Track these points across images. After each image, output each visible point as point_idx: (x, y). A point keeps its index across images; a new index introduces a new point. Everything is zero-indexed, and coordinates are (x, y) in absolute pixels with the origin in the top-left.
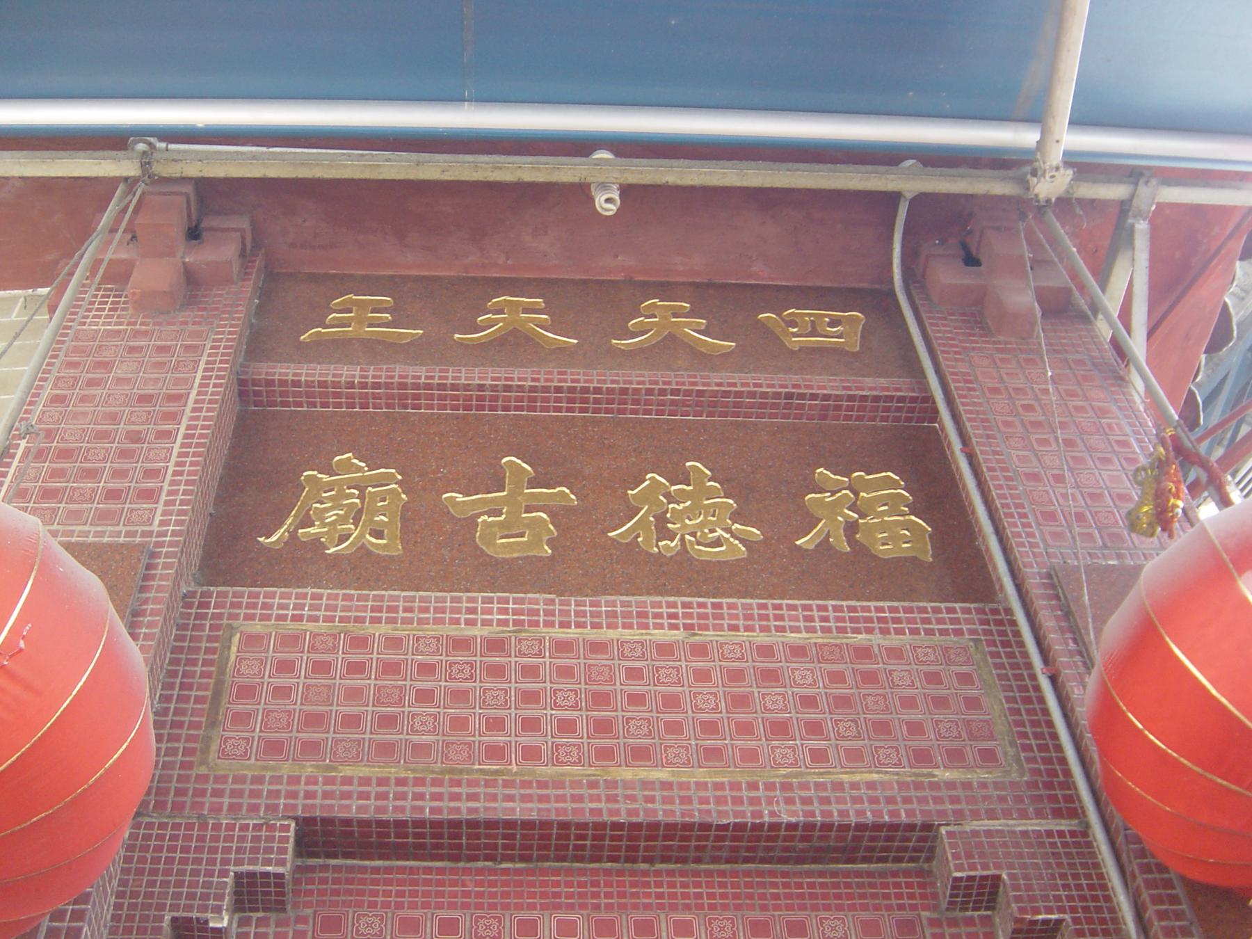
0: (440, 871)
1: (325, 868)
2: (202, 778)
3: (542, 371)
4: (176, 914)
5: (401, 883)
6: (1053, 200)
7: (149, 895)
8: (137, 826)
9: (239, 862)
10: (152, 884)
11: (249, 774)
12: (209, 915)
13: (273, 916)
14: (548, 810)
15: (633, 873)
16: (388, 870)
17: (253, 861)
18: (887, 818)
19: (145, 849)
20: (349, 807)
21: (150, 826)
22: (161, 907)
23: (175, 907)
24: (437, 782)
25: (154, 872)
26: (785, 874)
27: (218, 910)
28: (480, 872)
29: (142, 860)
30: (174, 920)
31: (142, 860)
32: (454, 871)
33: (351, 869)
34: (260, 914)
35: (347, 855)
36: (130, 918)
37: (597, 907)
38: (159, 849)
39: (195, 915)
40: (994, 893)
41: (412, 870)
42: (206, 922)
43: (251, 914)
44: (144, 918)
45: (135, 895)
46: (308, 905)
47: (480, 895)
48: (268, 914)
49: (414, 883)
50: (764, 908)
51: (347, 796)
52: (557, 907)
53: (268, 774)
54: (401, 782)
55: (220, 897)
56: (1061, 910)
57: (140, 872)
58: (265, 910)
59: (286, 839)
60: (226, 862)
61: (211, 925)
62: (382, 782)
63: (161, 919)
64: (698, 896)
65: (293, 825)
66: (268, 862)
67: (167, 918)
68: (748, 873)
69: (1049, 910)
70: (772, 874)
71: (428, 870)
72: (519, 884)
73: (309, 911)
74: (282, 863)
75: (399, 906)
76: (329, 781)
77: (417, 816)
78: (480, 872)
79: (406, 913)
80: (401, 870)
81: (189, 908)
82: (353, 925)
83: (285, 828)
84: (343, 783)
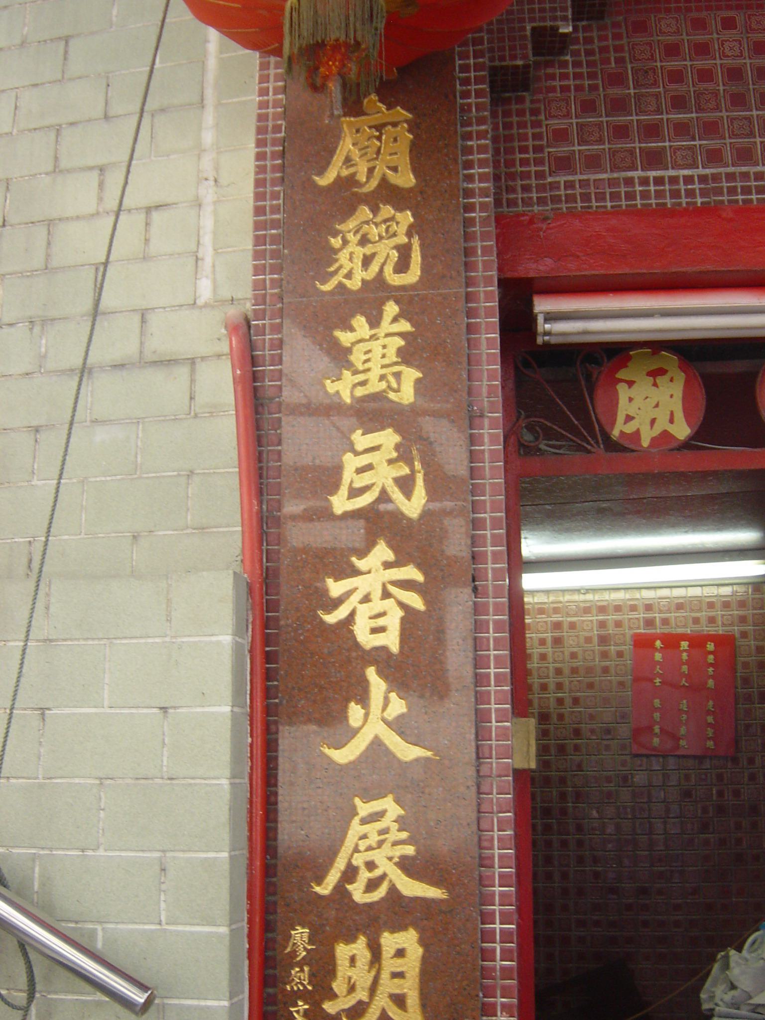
3: (594, 209)
4: (534, 25)
6: (381, 206)
12: (560, 23)
13: (594, 24)
18: (510, 832)
22: (521, 20)
23: (532, 20)
27: (565, 19)
30: (533, 29)
34: (584, 23)
39: (549, 23)
40: (467, 312)
42: (558, 29)
43: (578, 23)
48: (590, 22)
58: (588, 19)
61: (561, 31)
63: (523, 29)
67: (529, 28)
73: (621, 18)
75: (689, 10)
79: (694, 14)
82: (656, 25)
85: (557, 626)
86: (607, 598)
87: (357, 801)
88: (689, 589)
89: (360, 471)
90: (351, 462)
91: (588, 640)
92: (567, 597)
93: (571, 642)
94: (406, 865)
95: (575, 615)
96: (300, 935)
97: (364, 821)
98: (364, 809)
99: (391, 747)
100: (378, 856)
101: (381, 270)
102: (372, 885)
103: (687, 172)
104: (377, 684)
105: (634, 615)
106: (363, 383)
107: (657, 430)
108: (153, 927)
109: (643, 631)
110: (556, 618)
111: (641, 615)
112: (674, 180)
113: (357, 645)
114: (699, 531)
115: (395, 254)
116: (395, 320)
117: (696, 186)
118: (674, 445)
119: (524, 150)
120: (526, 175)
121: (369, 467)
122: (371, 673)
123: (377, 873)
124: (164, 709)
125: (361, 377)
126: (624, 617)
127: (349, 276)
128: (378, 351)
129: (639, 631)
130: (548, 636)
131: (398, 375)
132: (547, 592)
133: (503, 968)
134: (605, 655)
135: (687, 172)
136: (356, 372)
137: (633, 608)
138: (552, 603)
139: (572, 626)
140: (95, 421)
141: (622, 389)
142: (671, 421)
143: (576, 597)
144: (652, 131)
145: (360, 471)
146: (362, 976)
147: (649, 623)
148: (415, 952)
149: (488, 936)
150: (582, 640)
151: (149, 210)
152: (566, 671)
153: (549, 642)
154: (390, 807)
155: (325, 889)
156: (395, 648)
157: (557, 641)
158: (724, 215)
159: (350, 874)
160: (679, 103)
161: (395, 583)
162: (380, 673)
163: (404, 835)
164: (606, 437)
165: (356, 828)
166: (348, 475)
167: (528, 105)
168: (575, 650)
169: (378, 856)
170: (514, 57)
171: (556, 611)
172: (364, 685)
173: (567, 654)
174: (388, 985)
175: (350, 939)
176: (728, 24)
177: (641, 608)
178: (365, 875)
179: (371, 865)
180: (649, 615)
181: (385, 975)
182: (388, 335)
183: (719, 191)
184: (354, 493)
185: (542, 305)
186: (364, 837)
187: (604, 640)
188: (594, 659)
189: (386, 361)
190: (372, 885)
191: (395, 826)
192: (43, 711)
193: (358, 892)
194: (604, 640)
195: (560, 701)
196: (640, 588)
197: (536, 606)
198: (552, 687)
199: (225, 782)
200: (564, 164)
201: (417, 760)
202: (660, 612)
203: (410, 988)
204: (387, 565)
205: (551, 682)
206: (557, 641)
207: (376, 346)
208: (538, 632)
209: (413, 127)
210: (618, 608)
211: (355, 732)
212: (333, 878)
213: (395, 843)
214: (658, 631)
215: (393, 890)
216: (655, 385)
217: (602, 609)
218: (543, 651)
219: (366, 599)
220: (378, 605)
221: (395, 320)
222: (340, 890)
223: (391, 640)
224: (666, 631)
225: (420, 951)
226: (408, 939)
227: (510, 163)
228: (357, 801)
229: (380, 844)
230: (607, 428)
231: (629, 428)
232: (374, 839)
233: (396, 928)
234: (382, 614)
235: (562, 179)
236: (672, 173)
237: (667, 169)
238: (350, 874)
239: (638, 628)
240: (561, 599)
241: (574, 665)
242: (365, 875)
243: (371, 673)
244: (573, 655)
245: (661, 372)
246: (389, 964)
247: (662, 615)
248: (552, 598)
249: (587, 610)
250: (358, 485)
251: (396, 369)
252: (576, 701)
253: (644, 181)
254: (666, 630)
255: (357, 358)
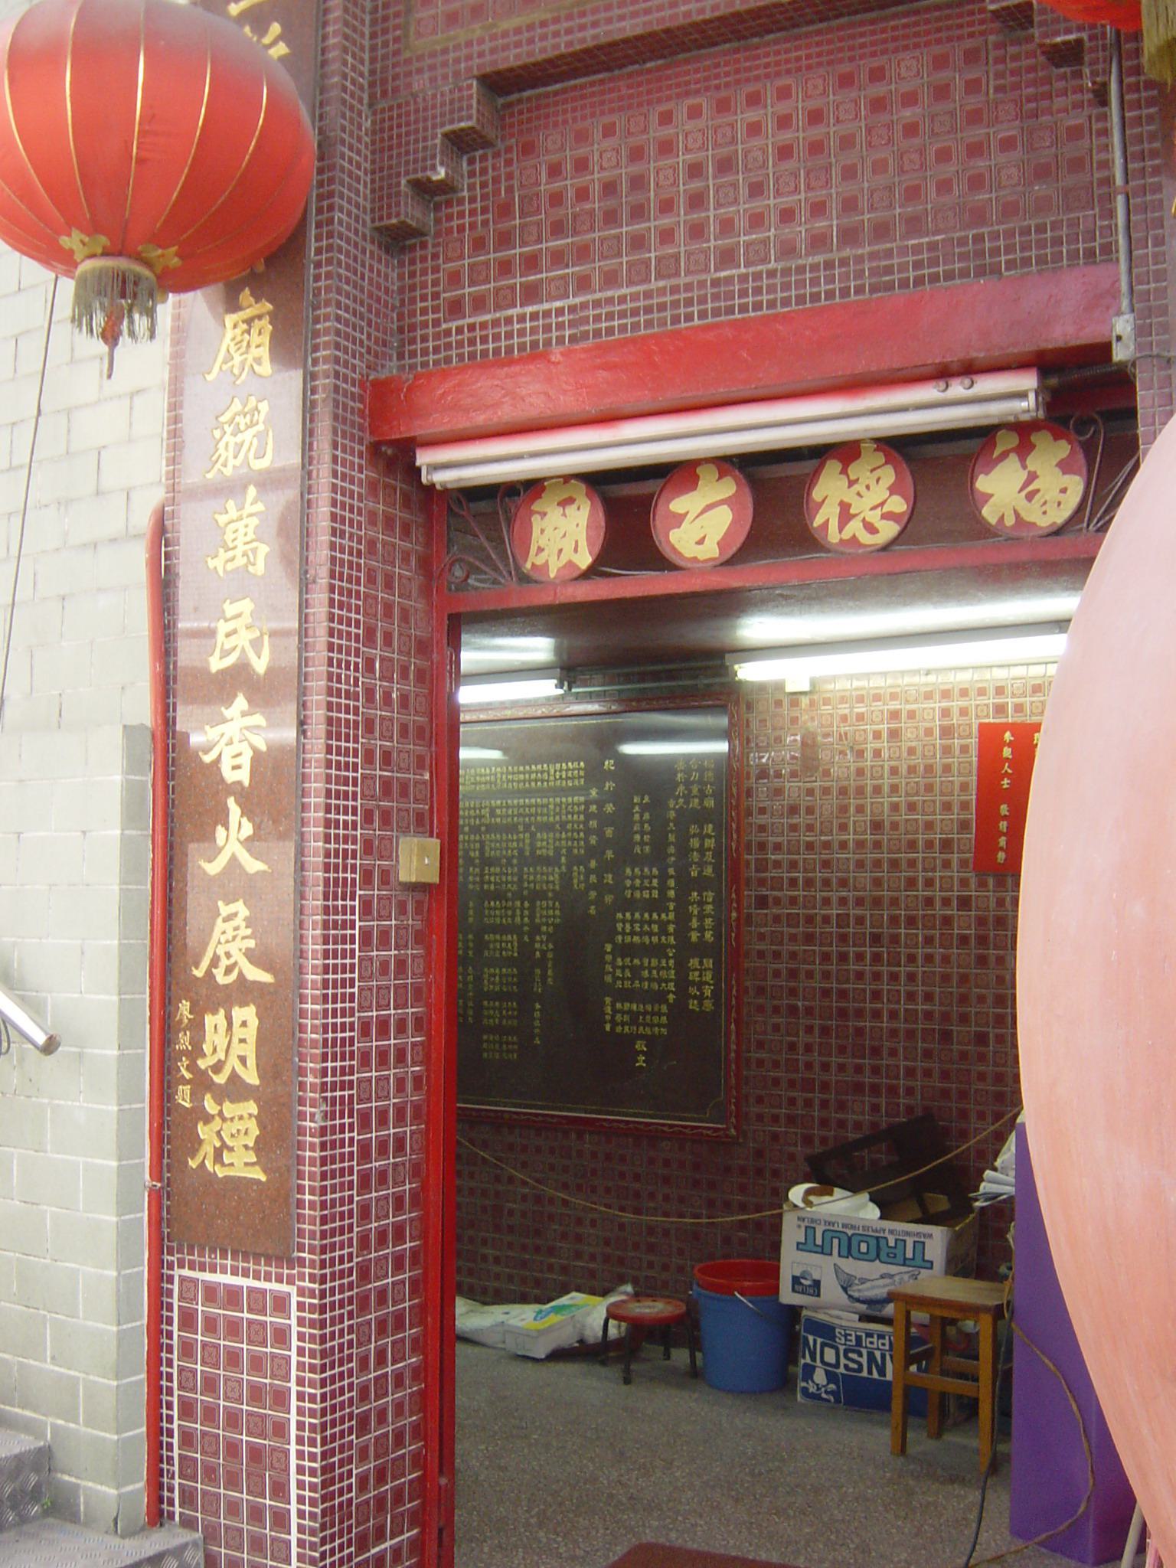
0: (602, 82)
1: (520, 101)
2: (408, 61)
5: (574, 100)
7: (390, 167)
8: (375, 113)
9: (443, 125)
10: (390, 157)
11: (438, 48)
12: (429, 173)
14: (651, 23)
15: (746, 49)
16: (564, 91)
17: (452, 122)
19: (382, 130)
20: (507, 59)
21: (383, 111)
22: (398, 175)
24: (570, 17)
25: (390, 148)
26: (873, 22)
28: (630, 75)
29: (382, 140)
31: (382, 140)
32: (611, 80)
33: (539, 97)
35: (533, 87)
36: (381, 188)
37: (718, 88)
38: (391, 128)
41: (582, 87)
44: (390, 187)
45: (381, 169)
46: (512, 135)
47: (631, 97)
49: (583, 97)
50: (852, 59)
51: (505, 48)
52: (687, 94)
53: (451, 45)
54: (543, 24)
55: (434, 157)
56: (1080, 29)
57: (382, 150)
59: (470, 97)
60: (434, 127)
62: (530, 27)
63: (399, 184)
64: (798, 59)
65: (475, 83)
66: (461, 120)
67: (403, 182)
68: (840, 28)
69: (1068, 31)
70: (862, 23)
71: (592, 84)
72: (659, 80)
74: (470, 118)
76: (493, 38)
77: (557, 53)
78: (630, 75)
80: (574, 89)
81: (415, 171)
83: (470, 87)
84: (503, 37)
85: (895, 715)
86: (952, 679)
87: (220, 903)
88: (995, 670)
89: (228, 635)
90: (223, 627)
91: (929, 732)
92: (907, 680)
93: (910, 735)
94: (249, 954)
95: (916, 701)
96: (185, 1007)
97: (225, 920)
98: (225, 910)
99: (243, 862)
100: (233, 948)
101: (246, 457)
102: (229, 970)
103: (558, 304)
104: (234, 810)
105: (982, 700)
106: (232, 559)
107: (564, 560)
108: (76, 995)
109: (991, 720)
110: (894, 706)
111: (991, 700)
112: (547, 314)
113: (222, 780)
114: (1049, 591)
115: (255, 441)
116: (254, 502)
117: (566, 318)
118: (576, 574)
119: (424, 298)
120: (425, 325)
121: (235, 632)
122: (231, 802)
123: (232, 961)
124: (84, 833)
125: (230, 554)
126: (971, 703)
127: (225, 465)
128: (242, 530)
129: (986, 721)
130: (884, 727)
131: (254, 551)
132: (851, 677)
133: (312, 1040)
134: (947, 750)
135: (558, 304)
136: (228, 549)
137: (982, 692)
138: (891, 687)
139: (911, 715)
140: (99, 590)
141: (535, 519)
142: (576, 550)
143: (916, 679)
144: (531, 263)
145: (228, 635)
146: (221, 1041)
147: (1000, 709)
148: (254, 1023)
149: (303, 1014)
150: (922, 733)
151: (132, 395)
152: (904, 770)
153: (885, 735)
154: (241, 908)
155: (199, 973)
156: (246, 783)
157: (894, 734)
158: (553, 359)
159: (215, 962)
160: (558, 229)
161: (247, 728)
162: (236, 801)
163: (249, 931)
164: (518, 568)
165: (220, 925)
166: (220, 637)
167: (430, 250)
168: (913, 744)
169: (233, 948)
170: (389, 217)
171: (894, 697)
172: (226, 811)
173: (904, 749)
174: (237, 1049)
175: (215, 1012)
176: (609, 131)
177: (991, 692)
178: (224, 962)
179: (228, 955)
180: (1000, 700)
181: (235, 1040)
182: (251, 515)
183: (585, 320)
184: (225, 654)
185: (424, 458)
186: (224, 933)
187: (947, 732)
188: (934, 756)
189: (248, 539)
190: (229, 970)
191: (243, 924)
192: (19, 834)
193: (221, 979)
194: (947, 732)
195: (895, 807)
196: (991, 667)
197: (872, 692)
198: (886, 789)
199: (116, 888)
200: (455, 308)
201: (257, 873)
202: (1013, 695)
203: (250, 1051)
204: (244, 714)
205: (886, 783)
206: (894, 734)
207: (240, 525)
208: (873, 722)
209: (274, 318)
210: (964, 693)
211: (220, 850)
212: (205, 964)
213: (243, 938)
214: (1010, 720)
215: (241, 975)
216: (564, 515)
217: (946, 694)
218: (878, 745)
219: (230, 743)
220: (236, 748)
221: (254, 502)
222: (209, 974)
223: (244, 776)
224: (1019, 720)
225: (257, 1022)
226: (246, 1014)
227: (413, 314)
228: (220, 903)
229: (234, 938)
230: (521, 562)
231: (539, 561)
232: (230, 934)
233: (243, 1004)
234: (239, 755)
235: (453, 325)
236: (546, 306)
237: (542, 302)
238: (215, 962)
239: (987, 716)
240: (900, 681)
241: (912, 763)
242: (224, 962)
243: (231, 802)
244: (911, 751)
245: (570, 501)
246: (238, 1032)
247: (1016, 700)
248: (890, 681)
249: (928, 696)
250: (227, 646)
251: (255, 544)
252: (912, 807)
253: (522, 319)
254: (1019, 719)
255: (229, 537)
